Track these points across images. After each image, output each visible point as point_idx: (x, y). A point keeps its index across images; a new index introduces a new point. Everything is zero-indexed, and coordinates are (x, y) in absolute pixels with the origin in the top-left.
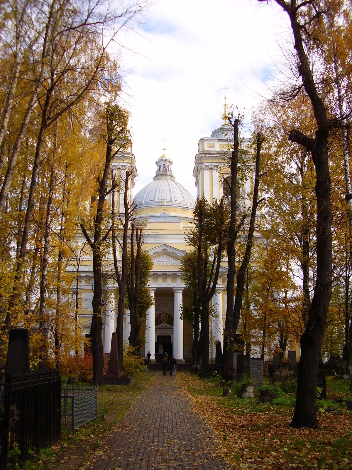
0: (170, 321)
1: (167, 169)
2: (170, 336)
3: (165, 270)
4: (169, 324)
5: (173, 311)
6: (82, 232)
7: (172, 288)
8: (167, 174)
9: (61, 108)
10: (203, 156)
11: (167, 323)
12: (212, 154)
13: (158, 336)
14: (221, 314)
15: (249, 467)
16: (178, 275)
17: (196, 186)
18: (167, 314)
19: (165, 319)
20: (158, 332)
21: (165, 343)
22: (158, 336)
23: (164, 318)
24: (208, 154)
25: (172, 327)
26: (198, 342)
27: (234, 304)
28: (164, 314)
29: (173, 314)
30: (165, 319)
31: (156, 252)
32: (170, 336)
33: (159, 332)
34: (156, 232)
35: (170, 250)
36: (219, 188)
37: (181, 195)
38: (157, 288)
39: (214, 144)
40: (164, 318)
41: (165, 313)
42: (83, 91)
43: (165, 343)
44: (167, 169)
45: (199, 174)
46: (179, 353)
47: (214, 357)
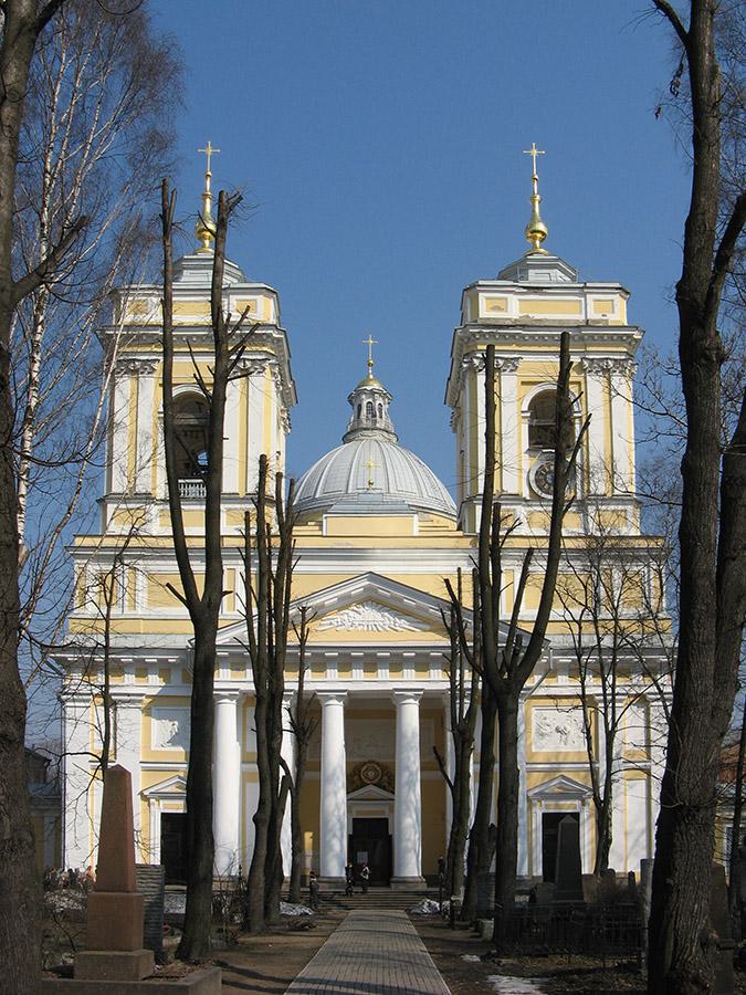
1: (378, 414)
2: (387, 819)
4: (384, 788)
5: (394, 756)
6: (225, 276)
8: (378, 425)
9: (128, 310)
10: (474, 334)
12: (501, 327)
13: (354, 819)
16: (408, 658)
17: (455, 430)
18: (377, 764)
21: (372, 837)
22: (354, 819)
23: (371, 774)
24: (488, 326)
25: (390, 795)
28: (369, 762)
29: (394, 763)
31: (348, 596)
32: (387, 819)
33: (359, 808)
34: (348, 544)
35: (384, 592)
36: (519, 423)
37: (414, 482)
38: (350, 693)
39: (506, 299)
41: (373, 762)
43: (372, 837)
44: (378, 414)
45: (463, 387)
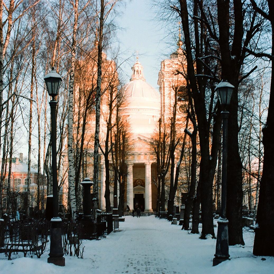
7: (144, 163)
11: (141, 185)
19: (139, 183)
21: (139, 199)
30: (139, 183)
38: (134, 163)
43: (139, 199)
46: (149, 205)
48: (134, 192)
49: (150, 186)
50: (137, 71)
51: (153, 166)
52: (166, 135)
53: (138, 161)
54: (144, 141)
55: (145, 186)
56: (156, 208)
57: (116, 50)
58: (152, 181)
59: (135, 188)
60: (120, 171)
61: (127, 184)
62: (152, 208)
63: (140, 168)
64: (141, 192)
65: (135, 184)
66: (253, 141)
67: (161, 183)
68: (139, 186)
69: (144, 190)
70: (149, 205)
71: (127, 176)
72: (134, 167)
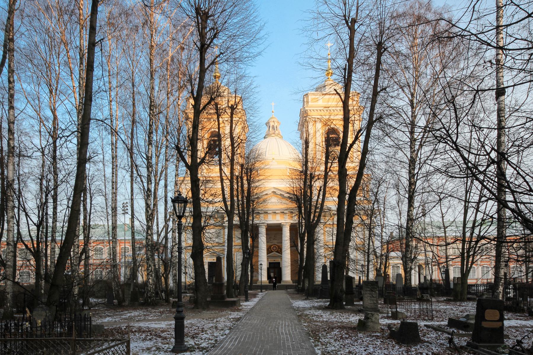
0: (280, 251)
3: (276, 211)
4: (279, 253)
5: (281, 243)
7: (281, 224)
11: (277, 252)
14: (341, 132)
15: (406, 335)
19: (275, 249)
20: (269, 259)
21: (275, 268)
26: (304, 267)
27: (329, 274)
30: (275, 249)
38: (268, 224)
40: (275, 248)
42: (226, 196)
43: (275, 268)
46: (287, 276)
47: (320, 279)
48: (268, 260)
49: (288, 251)
50: (273, 127)
51: (293, 228)
52: (314, 177)
53: (273, 220)
54: (280, 197)
55: (281, 249)
56: (297, 278)
57: (214, 237)
58: (291, 247)
59: (269, 255)
60: (249, 231)
61: (259, 259)
62: (291, 280)
63: (275, 231)
64: (277, 260)
65: (269, 251)
66: (495, 238)
67: (303, 209)
68: (274, 253)
69: (281, 257)
70: (287, 276)
71: (258, 235)
72: (267, 230)
